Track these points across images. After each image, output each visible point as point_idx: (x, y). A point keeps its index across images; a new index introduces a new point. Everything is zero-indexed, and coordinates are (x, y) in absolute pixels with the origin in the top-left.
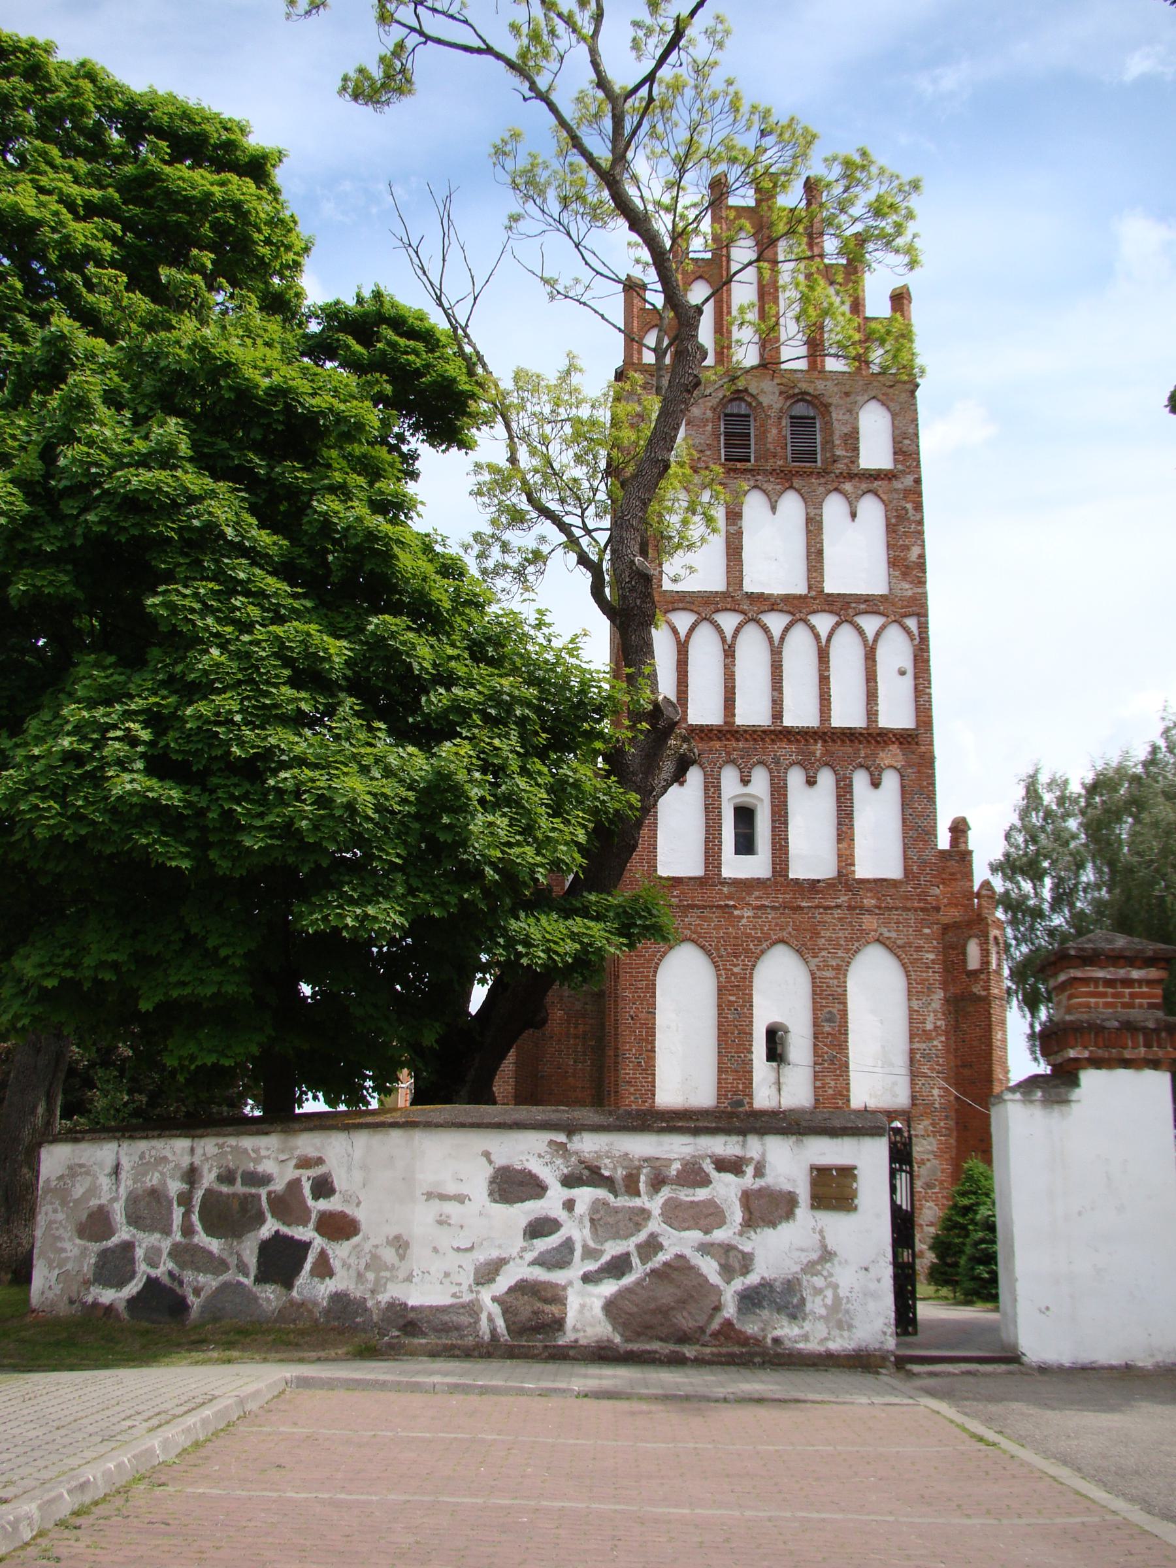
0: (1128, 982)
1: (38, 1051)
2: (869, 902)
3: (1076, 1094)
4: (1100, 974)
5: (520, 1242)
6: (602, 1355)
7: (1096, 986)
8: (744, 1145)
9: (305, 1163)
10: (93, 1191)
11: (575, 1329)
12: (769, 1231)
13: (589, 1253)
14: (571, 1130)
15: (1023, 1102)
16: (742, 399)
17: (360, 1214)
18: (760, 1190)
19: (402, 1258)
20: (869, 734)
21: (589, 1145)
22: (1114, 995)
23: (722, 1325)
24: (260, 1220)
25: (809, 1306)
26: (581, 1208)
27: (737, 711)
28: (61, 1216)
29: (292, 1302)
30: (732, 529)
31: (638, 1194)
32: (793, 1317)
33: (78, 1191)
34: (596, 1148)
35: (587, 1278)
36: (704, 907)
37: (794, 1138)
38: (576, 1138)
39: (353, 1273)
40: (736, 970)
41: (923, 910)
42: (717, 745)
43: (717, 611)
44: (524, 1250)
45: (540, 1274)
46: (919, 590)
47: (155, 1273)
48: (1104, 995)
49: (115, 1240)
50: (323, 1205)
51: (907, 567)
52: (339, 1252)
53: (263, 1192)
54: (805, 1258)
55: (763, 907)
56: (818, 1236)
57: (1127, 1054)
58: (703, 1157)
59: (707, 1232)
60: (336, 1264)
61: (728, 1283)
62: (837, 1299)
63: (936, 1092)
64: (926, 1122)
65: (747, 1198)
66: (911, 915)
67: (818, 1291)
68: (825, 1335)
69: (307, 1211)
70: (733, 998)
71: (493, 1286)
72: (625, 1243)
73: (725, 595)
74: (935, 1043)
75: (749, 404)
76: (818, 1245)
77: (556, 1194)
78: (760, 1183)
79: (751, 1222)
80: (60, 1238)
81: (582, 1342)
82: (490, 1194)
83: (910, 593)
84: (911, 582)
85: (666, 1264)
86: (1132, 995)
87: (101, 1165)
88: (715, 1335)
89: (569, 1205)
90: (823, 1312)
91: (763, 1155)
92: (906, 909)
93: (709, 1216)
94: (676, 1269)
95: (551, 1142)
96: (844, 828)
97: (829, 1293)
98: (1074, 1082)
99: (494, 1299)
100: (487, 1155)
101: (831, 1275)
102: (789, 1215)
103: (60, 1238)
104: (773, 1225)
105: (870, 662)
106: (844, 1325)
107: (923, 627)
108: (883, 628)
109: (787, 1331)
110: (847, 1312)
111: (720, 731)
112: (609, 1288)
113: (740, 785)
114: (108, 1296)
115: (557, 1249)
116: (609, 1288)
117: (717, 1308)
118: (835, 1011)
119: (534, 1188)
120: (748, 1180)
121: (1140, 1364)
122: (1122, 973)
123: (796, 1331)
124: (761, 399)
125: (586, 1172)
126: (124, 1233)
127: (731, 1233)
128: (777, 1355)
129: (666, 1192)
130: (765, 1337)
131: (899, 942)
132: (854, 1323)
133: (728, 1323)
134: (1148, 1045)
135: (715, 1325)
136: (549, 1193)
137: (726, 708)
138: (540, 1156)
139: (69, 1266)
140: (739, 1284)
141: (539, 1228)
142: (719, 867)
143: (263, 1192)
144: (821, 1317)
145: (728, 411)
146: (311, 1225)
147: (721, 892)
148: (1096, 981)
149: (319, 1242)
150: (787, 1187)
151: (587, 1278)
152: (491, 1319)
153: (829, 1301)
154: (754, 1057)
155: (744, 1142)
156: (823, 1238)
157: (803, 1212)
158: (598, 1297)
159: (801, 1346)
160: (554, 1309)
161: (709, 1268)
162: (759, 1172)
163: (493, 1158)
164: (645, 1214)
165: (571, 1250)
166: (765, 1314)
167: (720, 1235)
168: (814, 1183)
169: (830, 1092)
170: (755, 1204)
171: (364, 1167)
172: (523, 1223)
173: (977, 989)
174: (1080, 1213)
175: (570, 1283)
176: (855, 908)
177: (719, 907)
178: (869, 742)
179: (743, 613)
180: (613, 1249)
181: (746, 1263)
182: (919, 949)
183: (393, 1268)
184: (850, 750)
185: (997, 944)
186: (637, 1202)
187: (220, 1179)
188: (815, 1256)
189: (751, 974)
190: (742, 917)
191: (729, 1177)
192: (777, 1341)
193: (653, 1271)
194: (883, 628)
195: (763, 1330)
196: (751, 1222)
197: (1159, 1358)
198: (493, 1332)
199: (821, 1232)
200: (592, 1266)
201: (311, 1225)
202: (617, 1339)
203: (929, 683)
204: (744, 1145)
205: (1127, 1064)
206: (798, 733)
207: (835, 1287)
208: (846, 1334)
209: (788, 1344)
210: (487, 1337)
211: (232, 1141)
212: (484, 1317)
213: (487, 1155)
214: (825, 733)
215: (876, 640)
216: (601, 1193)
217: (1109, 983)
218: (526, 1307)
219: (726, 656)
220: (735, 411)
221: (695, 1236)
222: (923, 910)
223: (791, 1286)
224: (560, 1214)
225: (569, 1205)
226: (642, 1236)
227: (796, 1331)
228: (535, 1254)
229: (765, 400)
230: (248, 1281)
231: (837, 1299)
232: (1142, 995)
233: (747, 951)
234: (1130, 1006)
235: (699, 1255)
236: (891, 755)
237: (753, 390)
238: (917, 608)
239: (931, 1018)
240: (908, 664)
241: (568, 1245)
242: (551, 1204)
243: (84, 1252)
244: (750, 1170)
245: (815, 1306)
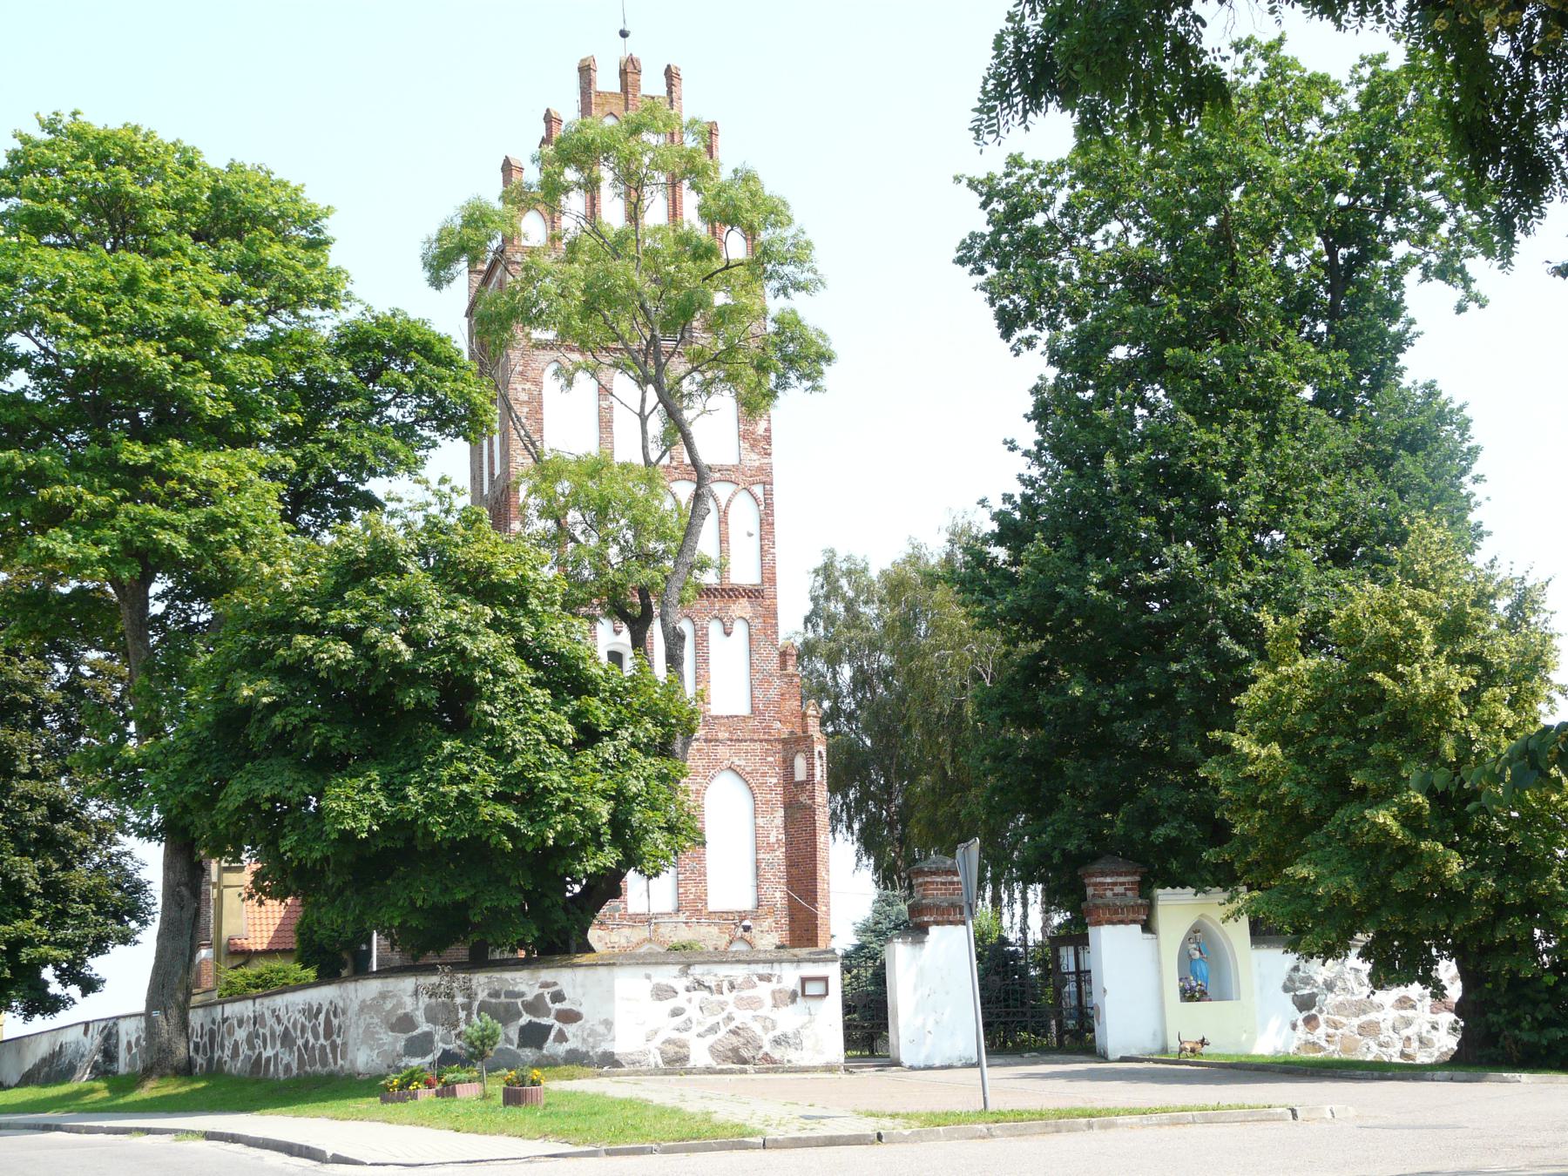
1: (182, 908)
2: (723, 735)
3: (928, 938)
4: (939, 879)
6: (709, 1071)
9: (545, 985)
10: (400, 1004)
13: (699, 1023)
17: (582, 1010)
19: (609, 1030)
20: (723, 590)
24: (520, 1015)
28: (376, 1020)
29: (543, 1056)
33: (388, 1005)
35: (699, 1035)
39: (580, 1039)
41: (767, 741)
45: (675, 1035)
46: (766, 461)
47: (447, 1047)
49: (419, 1031)
50: (558, 1006)
51: (755, 440)
52: (570, 1029)
53: (519, 1001)
57: (951, 918)
60: (569, 1035)
63: (778, 894)
64: (770, 920)
66: (758, 745)
69: (549, 1010)
74: (777, 853)
80: (377, 1033)
83: (757, 464)
84: (759, 454)
87: (404, 990)
89: (690, 1001)
92: (752, 740)
93: (753, 1003)
96: (702, 672)
98: (926, 932)
103: (377, 1033)
105: (723, 525)
106: (820, 1052)
107: (768, 494)
108: (734, 495)
112: (711, 1039)
113: (613, 634)
114: (415, 1062)
116: (711, 1039)
122: (949, 878)
126: (424, 1027)
129: (735, 993)
131: (748, 769)
139: (386, 1047)
143: (519, 1001)
146: (552, 1016)
149: (557, 1025)
160: (684, 1050)
161: (757, 1028)
164: (726, 1003)
169: (692, 897)
170: (777, 996)
171: (583, 986)
173: (803, 798)
176: (711, 741)
178: (723, 596)
180: (711, 1021)
182: (764, 774)
183: (604, 1035)
184: (706, 603)
185: (821, 757)
187: (490, 995)
194: (734, 495)
200: (701, 1029)
201: (552, 1016)
203: (774, 543)
205: (951, 923)
211: (497, 975)
215: (728, 506)
216: (706, 994)
217: (942, 883)
218: (671, 1050)
221: (750, 1013)
222: (767, 741)
226: (724, 1014)
230: (513, 1048)
236: (742, 608)
238: (764, 477)
239: (774, 833)
240: (755, 528)
242: (680, 1001)
243: (396, 1040)
244: (775, 980)
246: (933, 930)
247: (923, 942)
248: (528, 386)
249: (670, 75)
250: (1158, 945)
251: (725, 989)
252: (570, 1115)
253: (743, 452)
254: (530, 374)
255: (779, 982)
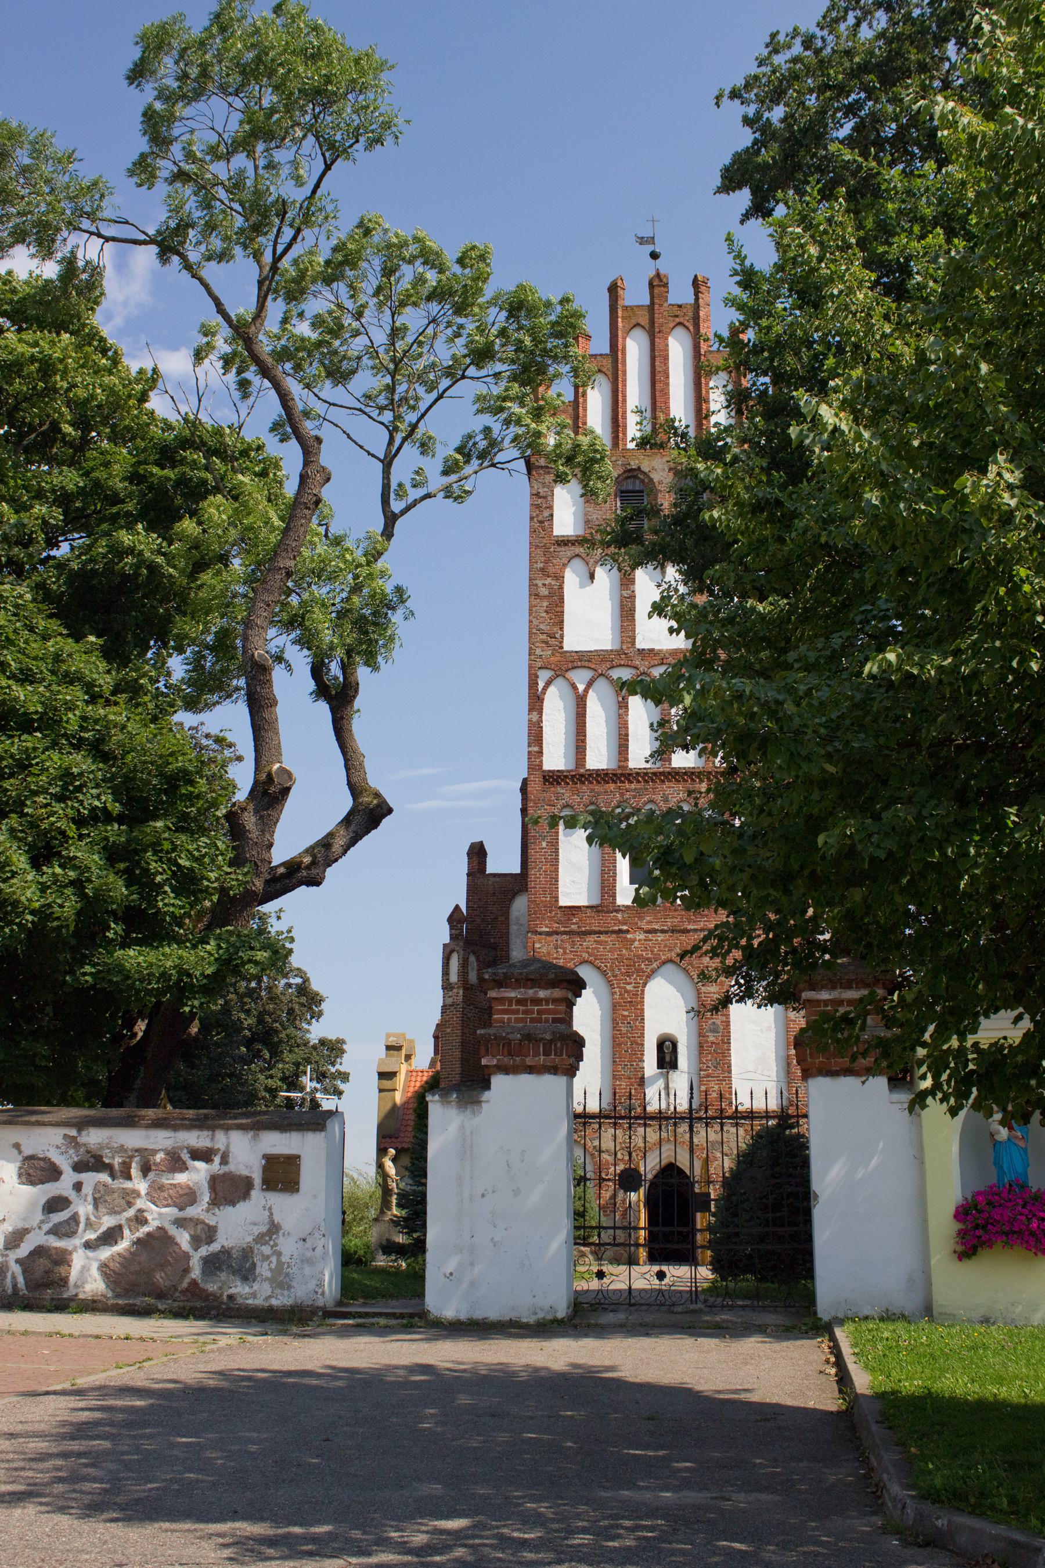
0: (537, 1001)
3: (486, 1096)
4: (512, 994)
5: (39, 1216)
7: (510, 1004)
8: (213, 1139)
11: (76, 1286)
12: (231, 1208)
14: (82, 1125)
15: (442, 1102)
16: (636, 477)
18: (224, 1175)
21: (94, 1137)
22: (525, 1012)
23: (190, 1284)
25: (258, 1270)
26: (87, 1189)
27: (630, 756)
30: (625, 593)
31: (129, 1178)
32: (245, 1279)
34: (99, 1141)
35: (88, 1245)
36: (600, 933)
37: (251, 1133)
38: (84, 1133)
40: (629, 987)
42: (612, 786)
43: (613, 667)
44: (42, 1222)
48: (517, 1012)
54: (257, 1231)
55: (655, 931)
56: (267, 1213)
57: (529, 1061)
58: (181, 1148)
59: (181, 1209)
61: (196, 1250)
62: (280, 1263)
65: (214, 1181)
67: (266, 1258)
68: (269, 1293)
70: (626, 1013)
71: (18, 1251)
72: (118, 1217)
73: (619, 653)
75: (643, 481)
76: (267, 1220)
77: (69, 1177)
78: (225, 1169)
79: (216, 1202)
81: (81, 1296)
82: (20, 1176)
85: (149, 1234)
86: (539, 1012)
88: (184, 1292)
89: (78, 1187)
90: (269, 1274)
91: (228, 1146)
94: (156, 1238)
95: (65, 1136)
97: (274, 1259)
98: (486, 1086)
99: (17, 1261)
100: (17, 1146)
101: (276, 1245)
102: (246, 1195)
104: (233, 1204)
109: (239, 1289)
110: (288, 1274)
111: (615, 775)
112: (106, 1253)
115: (67, 1222)
117: (187, 1270)
118: (718, 1022)
119: (53, 1173)
120: (216, 1166)
121: (525, 1320)
123: (247, 1290)
124: (652, 476)
125: (92, 1160)
127: (199, 1210)
128: (229, 1308)
130: (222, 1295)
132: (294, 1284)
133: (194, 1283)
134: (546, 1054)
135: (185, 1284)
136: (63, 1177)
137: (620, 753)
138: (58, 1147)
140: (204, 1251)
141: (55, 1205)
142: (614, 896)
144: (267, 1279)
145: (624, 488)
147: (616, 919)
148: (510, 1000)
150: (245, 1172)
151: (88, 1245)
152: (14, 1277)
153: (273, 1266)
154: (645, 1065)
155: (213, 1136)
156: (271, 1214)
157: (255, 1193)
158: (96, 1260)
159: (250, 1302)
161: (183, 1239)
162: (224, 1161)
163: (23, 1148)
165: (78, 1224)
166: (223, 1276)
167: (192, 1212)
168: (265, 1169)
172: (43, 1200)
174: (483, 1196)
175: (75, 1248)
177: (613, 932)
179: (636, 668)
180: (108, 1222)
181: (210, 1234)
186: (128, 1185)
188: (264, 1229)
189: (643, 991)
190: (634, 940)
191: (200, 1165)
192: (231, 1297)
193: (139, 1239)
195: (220, 1288)
196: (216, 1202)
197: (541, 1315)
198: (15, 1286)
199: (270, 1209)
200: (92, 1236)
202: (110, 1294)
204: (213, 1139)
205: (531, 1070)
206: (685, 773)
207: (279, 1254)
208: (286, 1293)
209: (240, 1300)
210: (10, 1291)
212: (9, 1275)
213: (17, 1146)
214: (710, 773)
216: (104, 1177)
217: (520, 1002)
219: (620, 707)
220: (630, 488)
223: (247, 1253)
224: (72, 1195)
225: (78, 1187)
226: (131, 1213)
227: (246, 1290)
228: (51, 1225)
229: (655, 477)
231: (280, 1263)
232: (548, 1012)
233: (639, 970)
234: (539, 1020)
235: (174, 1227)
237: (645, 468)
241: (75, 1218)
242: (63, 1187)
244: (217, 1160)
245: (264, 1270)
246: (498, 1081)
247: (478, 1102)
248: (549, 581)
249: (696, 284)
250: (920, 1127)
251: (134, 1172)
252: (866, 1318)
253: (379, 419)
254: (551, 570)
255: (224, 1161)
